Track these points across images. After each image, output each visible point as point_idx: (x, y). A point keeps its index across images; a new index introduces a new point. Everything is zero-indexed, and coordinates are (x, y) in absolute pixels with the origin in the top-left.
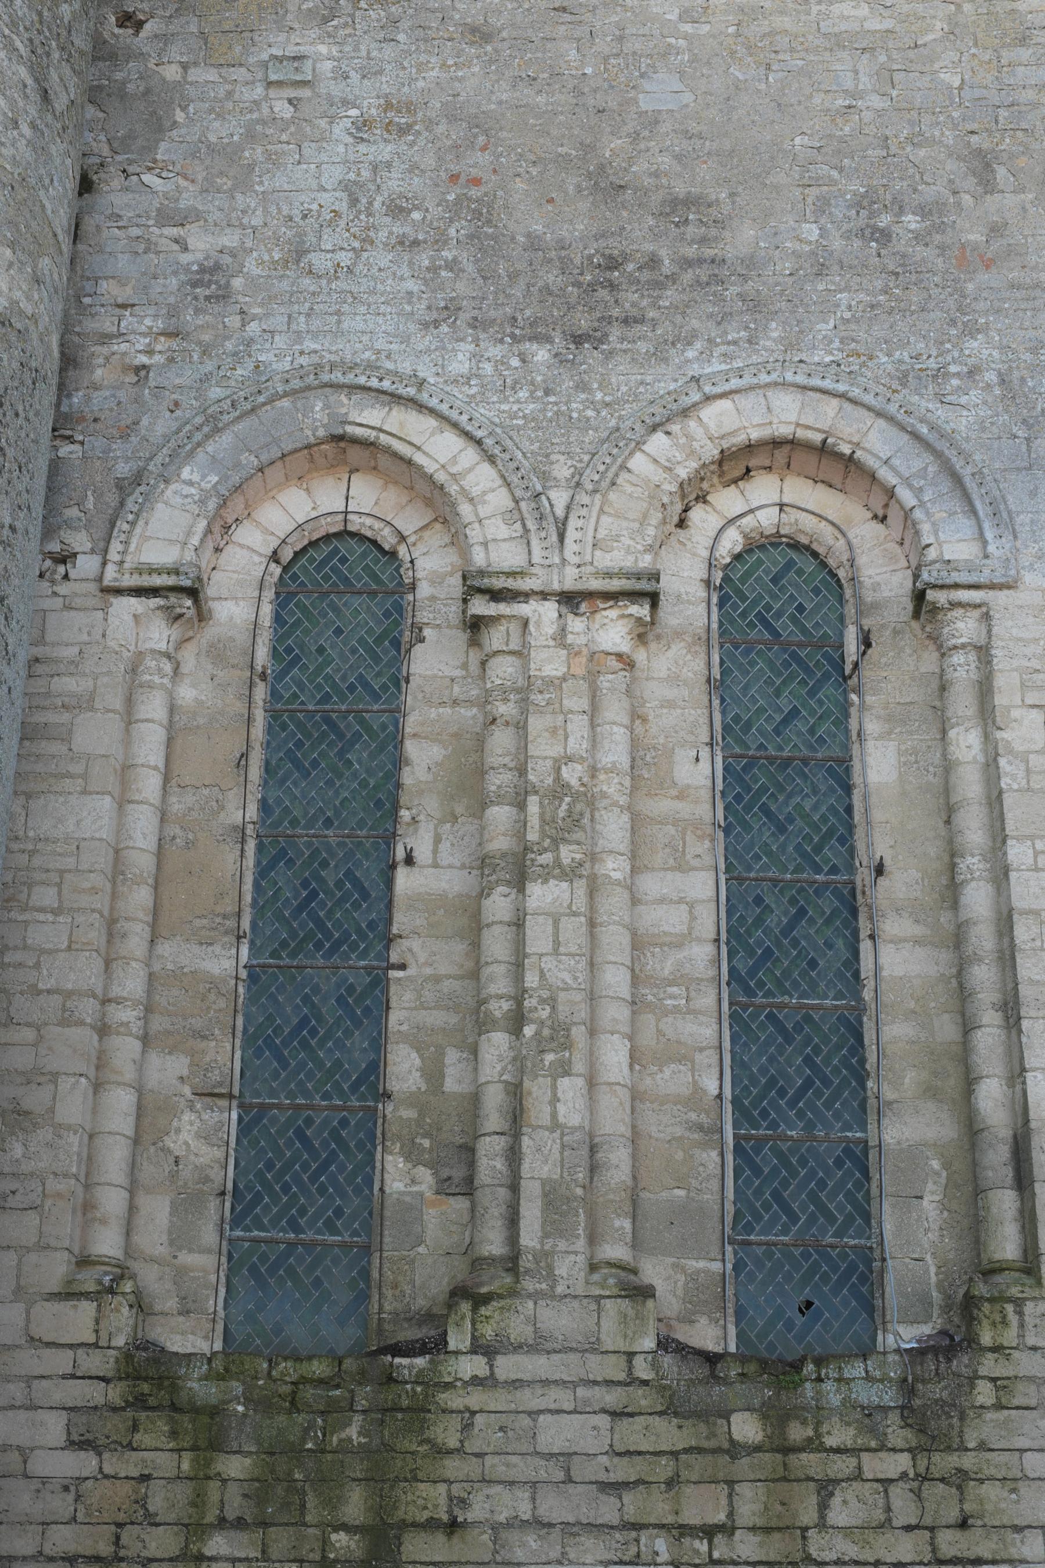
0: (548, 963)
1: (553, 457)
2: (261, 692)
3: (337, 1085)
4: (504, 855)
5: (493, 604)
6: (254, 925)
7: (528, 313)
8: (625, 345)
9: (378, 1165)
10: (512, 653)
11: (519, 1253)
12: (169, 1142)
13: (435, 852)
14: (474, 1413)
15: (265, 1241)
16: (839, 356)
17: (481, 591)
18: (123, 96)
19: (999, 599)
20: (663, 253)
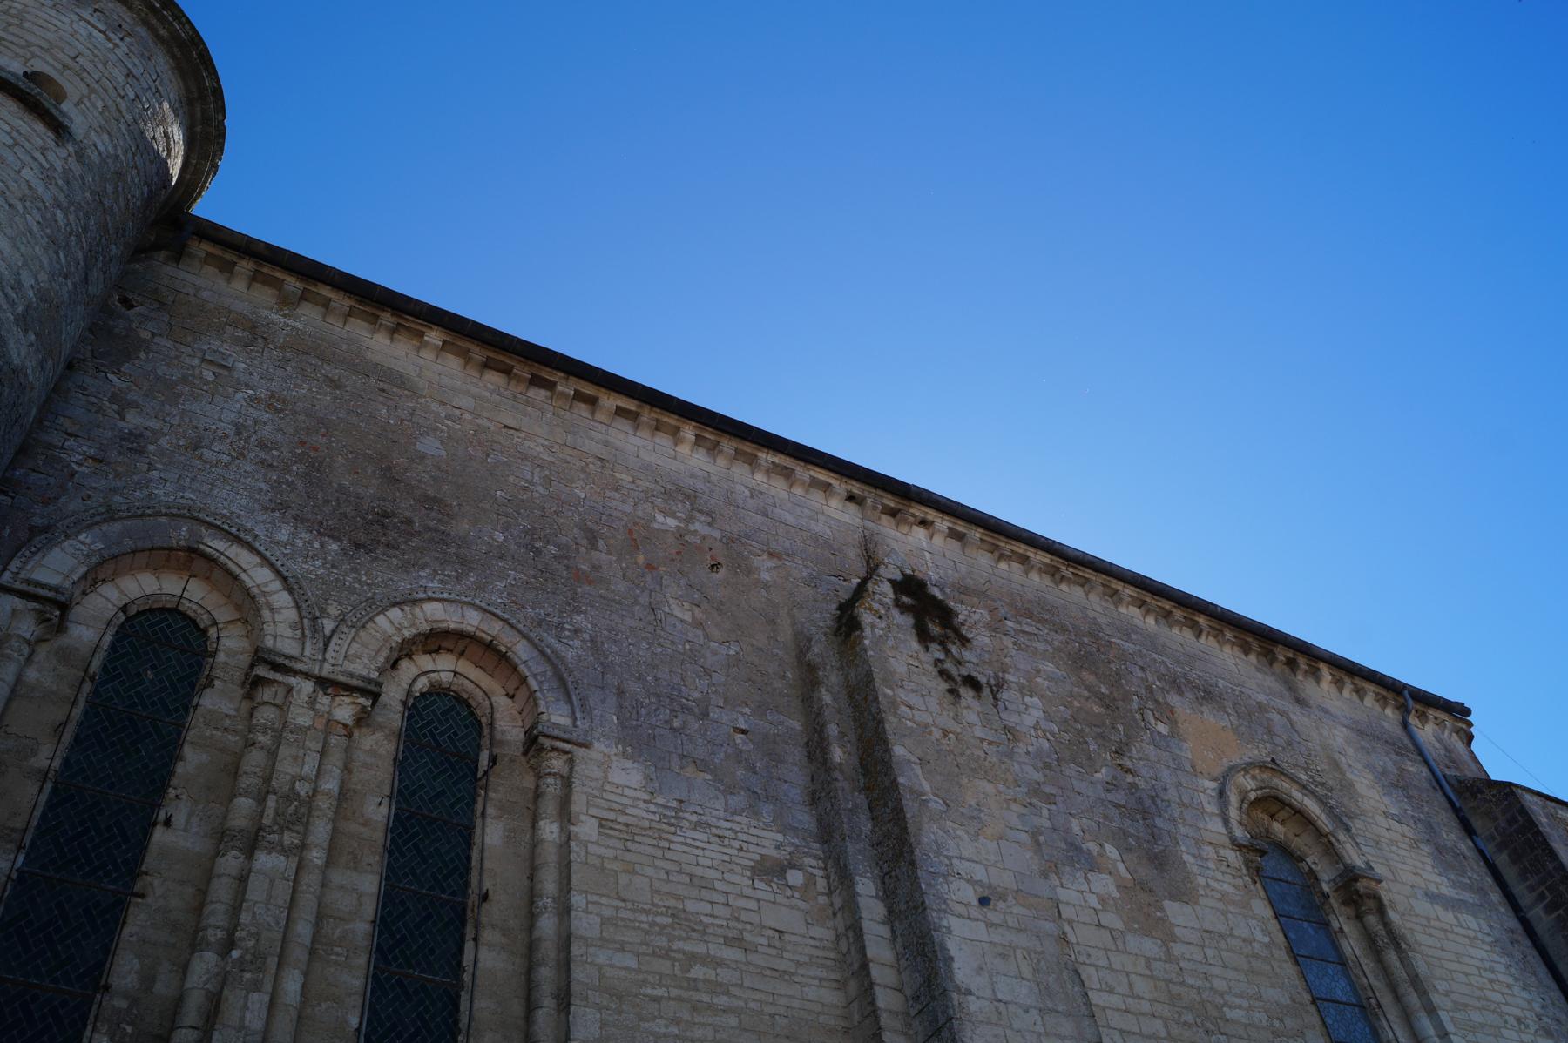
1: (329, 602)
4: (242, 831)
5: (272, 672)
6: (33, 843)
7: (330, 523)
8: (385, 557)
10: (275, 705)
13: (187, 822)
16: (506, 601)
17: (266, 662)
19: (580, 752)
20: (416, 519)
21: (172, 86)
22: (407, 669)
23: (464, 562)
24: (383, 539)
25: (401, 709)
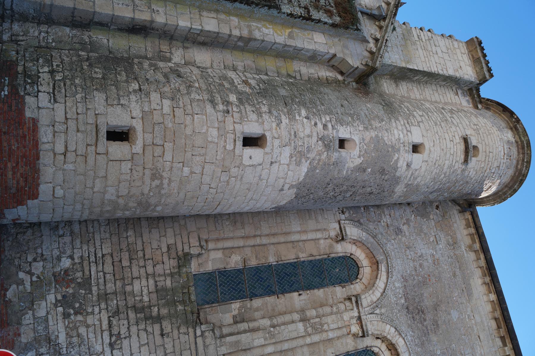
0: (287, 330)
2: (326, 256)
3: (251, 288)
4: (306, 315)
6: (280, 264)
9: (237, 301)
11: (224, 337)
12: (233, 255)
14: (188, 334)
15: (216, 279)
17: (357, 299)
18: (425, 208)
20: (427, 322)
21: (506, 179)
22: (378, 343)
23: (423, 344)
24: (414, 315)
25: (365, 347)
